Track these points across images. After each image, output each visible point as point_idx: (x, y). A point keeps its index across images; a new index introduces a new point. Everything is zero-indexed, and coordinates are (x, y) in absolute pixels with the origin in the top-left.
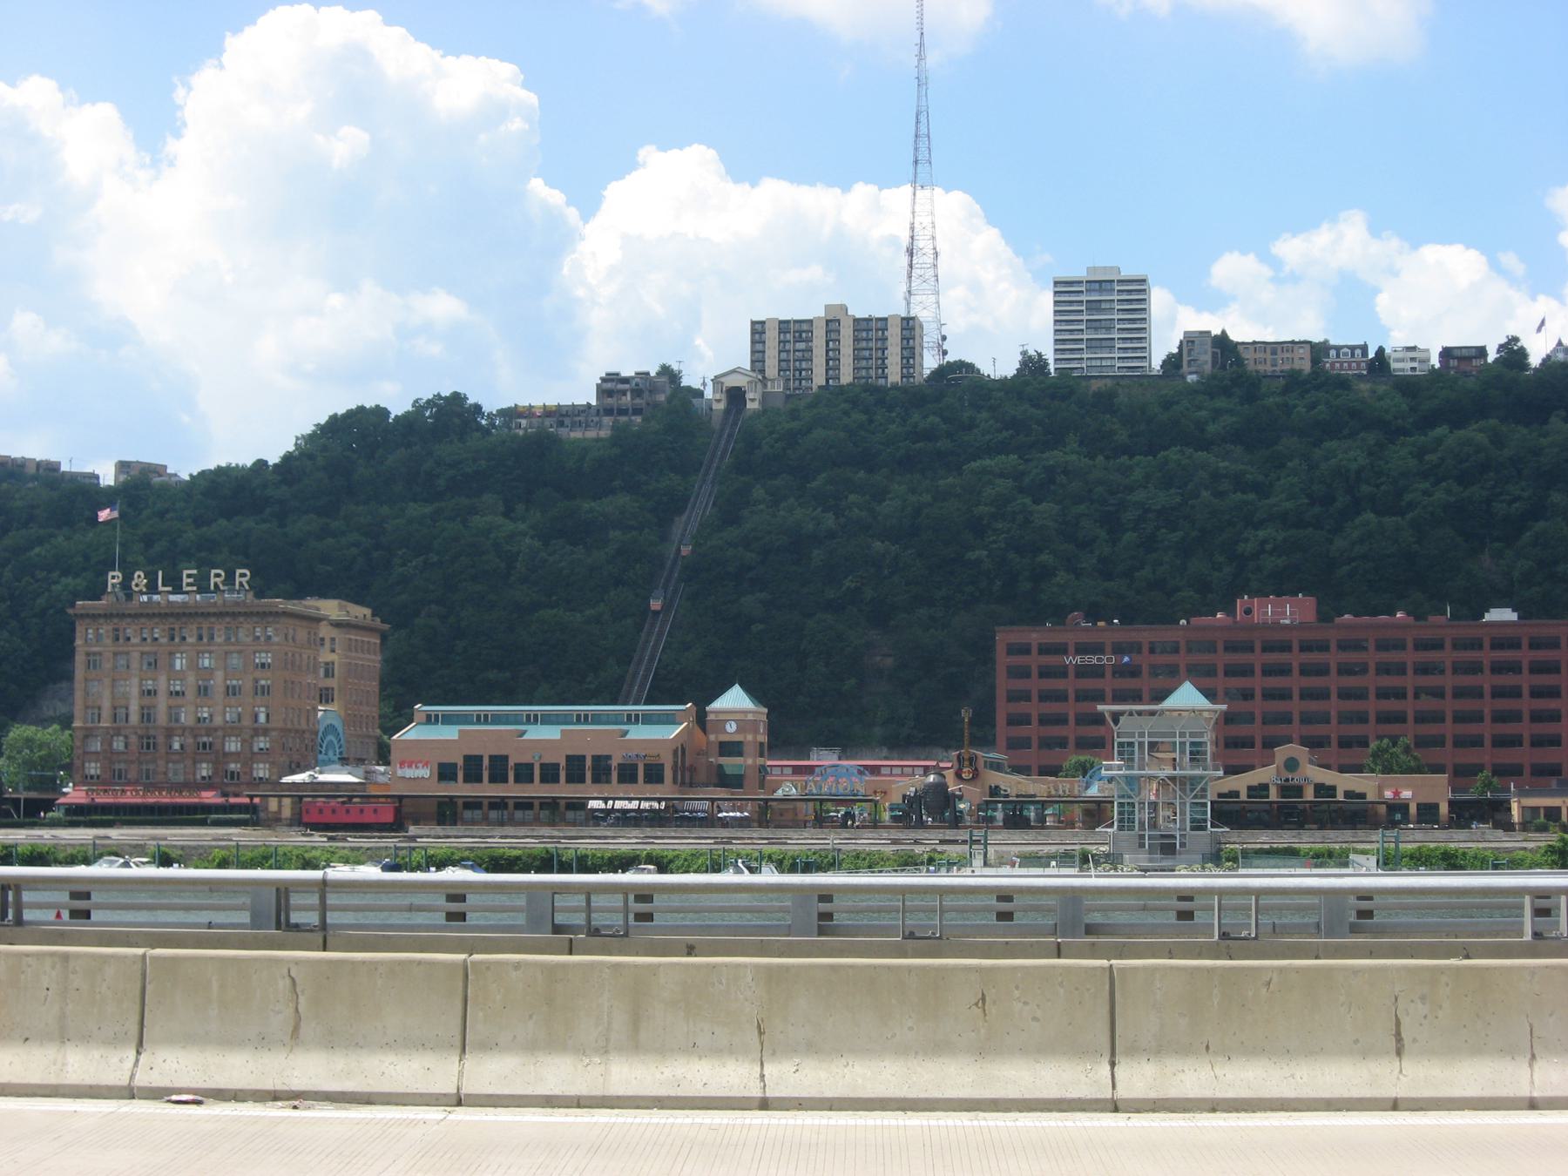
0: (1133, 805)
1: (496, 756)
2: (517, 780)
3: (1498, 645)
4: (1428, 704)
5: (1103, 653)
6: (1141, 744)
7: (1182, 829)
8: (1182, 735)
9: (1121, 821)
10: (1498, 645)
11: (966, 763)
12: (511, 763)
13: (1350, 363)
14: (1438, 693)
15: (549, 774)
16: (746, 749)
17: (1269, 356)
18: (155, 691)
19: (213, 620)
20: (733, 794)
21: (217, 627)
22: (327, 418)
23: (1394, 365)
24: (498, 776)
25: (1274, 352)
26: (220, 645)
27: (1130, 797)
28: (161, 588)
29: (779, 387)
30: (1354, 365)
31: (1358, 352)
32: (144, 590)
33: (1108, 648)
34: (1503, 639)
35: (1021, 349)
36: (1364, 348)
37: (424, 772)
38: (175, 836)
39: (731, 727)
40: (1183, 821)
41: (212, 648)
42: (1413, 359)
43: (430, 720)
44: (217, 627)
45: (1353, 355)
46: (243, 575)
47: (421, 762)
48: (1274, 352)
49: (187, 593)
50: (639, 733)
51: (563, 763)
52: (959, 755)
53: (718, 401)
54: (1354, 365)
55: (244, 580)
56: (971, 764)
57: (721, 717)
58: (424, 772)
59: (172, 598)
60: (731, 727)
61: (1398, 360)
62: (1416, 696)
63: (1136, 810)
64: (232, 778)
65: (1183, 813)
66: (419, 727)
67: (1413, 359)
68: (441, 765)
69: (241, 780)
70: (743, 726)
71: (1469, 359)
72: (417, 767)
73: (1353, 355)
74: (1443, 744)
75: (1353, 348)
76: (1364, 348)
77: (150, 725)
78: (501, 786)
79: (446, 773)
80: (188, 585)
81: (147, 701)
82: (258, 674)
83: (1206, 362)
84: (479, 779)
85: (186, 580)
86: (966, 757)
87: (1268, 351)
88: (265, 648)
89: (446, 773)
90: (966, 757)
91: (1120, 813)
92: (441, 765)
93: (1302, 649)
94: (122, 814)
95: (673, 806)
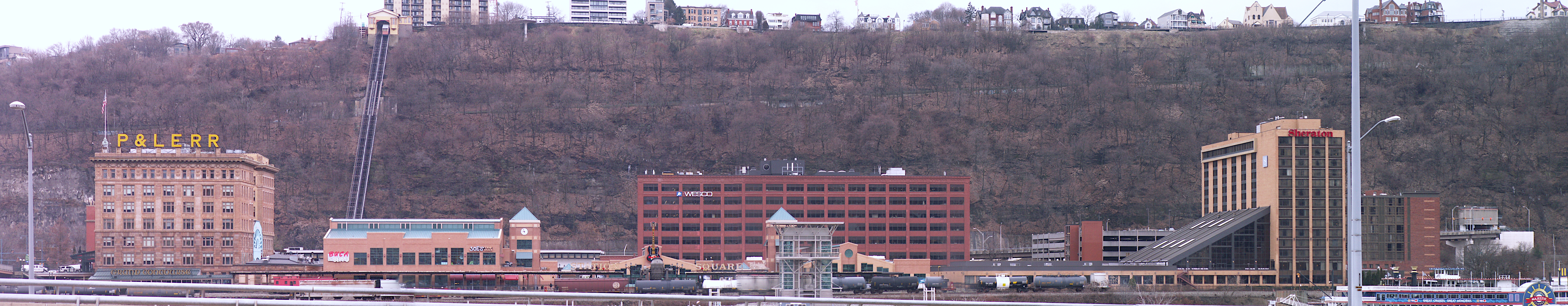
0: (791, 275)
1: (456, 249)
2: (485, 262)
3: (893, 188)
4: (876, 220)
5: (698, 190)
6: (796, 242)
7: (818, 287)
8: (818, 238)
9: (785, 284)
10: (893, 188)
11: (654, 252)
12: (401, 253)
13: (743, 21)
14: (881, 214)
15: (425, 259)
16: (534, 244)
17: (697, 15)
18: (193, 208)
19: (193, 165)
20: (527, 270)
21: (156, 169)
22: (297, 39)
23: (770, 24)
24: (393, 261)
25: (700, 13)
26: (198, 181)
27: (790, 271)
28: (155, 145)
29: (409, 22)
30: (745, 22)
31: (748, 15)
32: (144, 146)
33: (702, 188)
34: (897, 186)
35: (547, 4)
36: (751, 13)
37: (346, 259)
38: (275, 293)
39: (524, 232)
40: (818, 283)
41: (193, 183)
42: (780, 21)
43: (340, 227)
44: (156, 169)
45: (745, 17)
46: (195, 138)
47: (343, 252)
48: (700, 13)
49: (173, 148)
50: (411, 236)
51: (369, 253)
52: (649, 247)
53: (372, 29)
54: (745, 22)
55: (214, 141)
56: (656, 253)
57: (518, 226)
58: (346, 259)
59: (163, 151)
60: (524, 232)
61: (771, 21)
62: (870, 216)
63: (794, 277)
64: (188, 263)
65: (818, 279)
66: (333, 232)
67: (780, 21)
68: (356, 254)
69: (214, 264)
70: (532, 230)
71: (810, 21)
72: (341, 256)
73: (745, 17)
74: (698, 242)
75: (745, 13)
76: (751, 13)
77: (151, 230)
78: (395, 266)
79: (360, 259)
80: (176, 143)
81: (148, 215)
82: (225, 199)
83: (661, 17)
84: (381, 263)
85: (173, 140)
86: (653, 249)
87: (697, 12)
88: (229, 183)
89: (360, 259)
90: (653, 249)
91: (785, 279)
92: (356, 254)
93: (809, 189)
94: (1131, 277)
95: (501, 277)
